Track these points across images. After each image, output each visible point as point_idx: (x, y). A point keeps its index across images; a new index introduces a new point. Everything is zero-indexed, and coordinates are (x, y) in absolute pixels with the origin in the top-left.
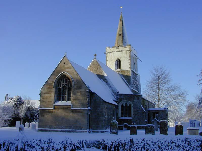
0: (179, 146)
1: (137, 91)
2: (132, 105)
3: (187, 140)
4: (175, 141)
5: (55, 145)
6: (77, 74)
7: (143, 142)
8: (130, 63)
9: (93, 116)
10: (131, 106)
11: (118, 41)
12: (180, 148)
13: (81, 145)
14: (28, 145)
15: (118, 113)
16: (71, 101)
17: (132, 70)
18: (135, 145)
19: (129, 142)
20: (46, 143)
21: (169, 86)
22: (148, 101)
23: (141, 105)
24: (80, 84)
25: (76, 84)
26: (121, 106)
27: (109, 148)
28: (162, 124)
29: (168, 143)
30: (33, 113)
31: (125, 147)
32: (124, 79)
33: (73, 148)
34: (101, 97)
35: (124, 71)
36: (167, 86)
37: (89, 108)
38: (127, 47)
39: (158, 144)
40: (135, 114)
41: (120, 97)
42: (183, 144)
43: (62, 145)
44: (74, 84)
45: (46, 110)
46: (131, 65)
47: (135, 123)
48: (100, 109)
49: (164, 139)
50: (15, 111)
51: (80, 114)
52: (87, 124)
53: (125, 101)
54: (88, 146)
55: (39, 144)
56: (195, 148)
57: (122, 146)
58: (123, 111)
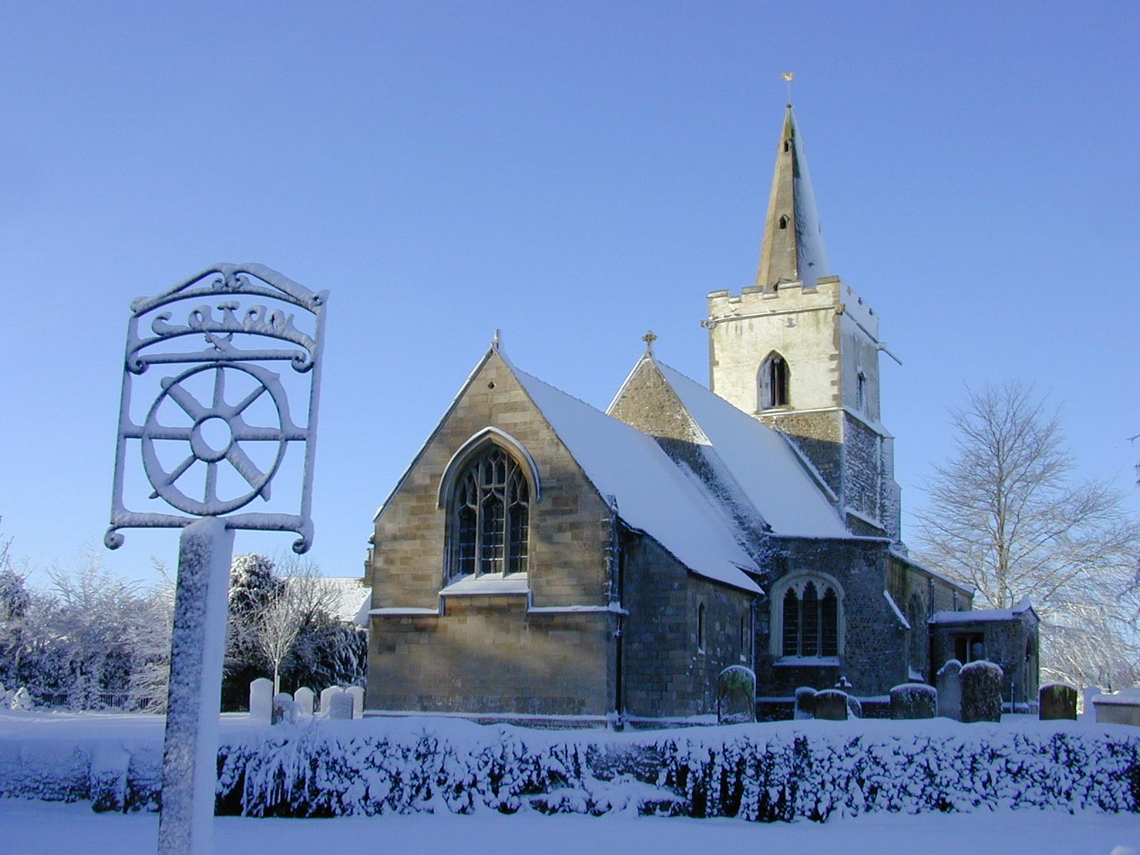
0: (1024, 772)
1: (876, 523)
2: (840, 593)
3: (1063, 743)
4: (1005, 747)
5: (451, 766)
6: (556, 441)
7: (852, 750)
8: (835, 376)
9: (635, 646)
10: (835, 600)
11: (771, 258)
12: (1029, 782)
13: (567, 768)
14: (331, 766)
15: (768, 636)
16: (524, 575)
17: (847, 413)
18: (814, 767)
19: (788, 752)
20: (411, 755)
21: (1059, 495)
22: (930, 577)
23: (886, 594)
24: (571, 489)
25: (551, 488)
26: (785, 601)
27: (695, 780)
28: (971, 682)
29: (973, 756)
30: (331, 645)
31: (772, 777)
32: (806, 460)
33: (534, 777)
34: (676, 555)
35: (805, 418)
36: (1043, 494)
37: (615, 607)
38: (818, 288)
39: (925, 764)
40: (854, 643)
41: (778, 555)
42: (1045, 762)
43: (482, 764)
44: (541, 489)
45: (404, 621)
46: (839, 383)
47: (847, 684)
48: (670, 611)
49: (952, 739)
50: (237, 634)
51: (573, 637)
52: (608, 685)
53: (804, 571)
54: (603, 769)
55: (377, 762)
56: (1100, 783)
57: (757, 772)
58: (796, 625)
